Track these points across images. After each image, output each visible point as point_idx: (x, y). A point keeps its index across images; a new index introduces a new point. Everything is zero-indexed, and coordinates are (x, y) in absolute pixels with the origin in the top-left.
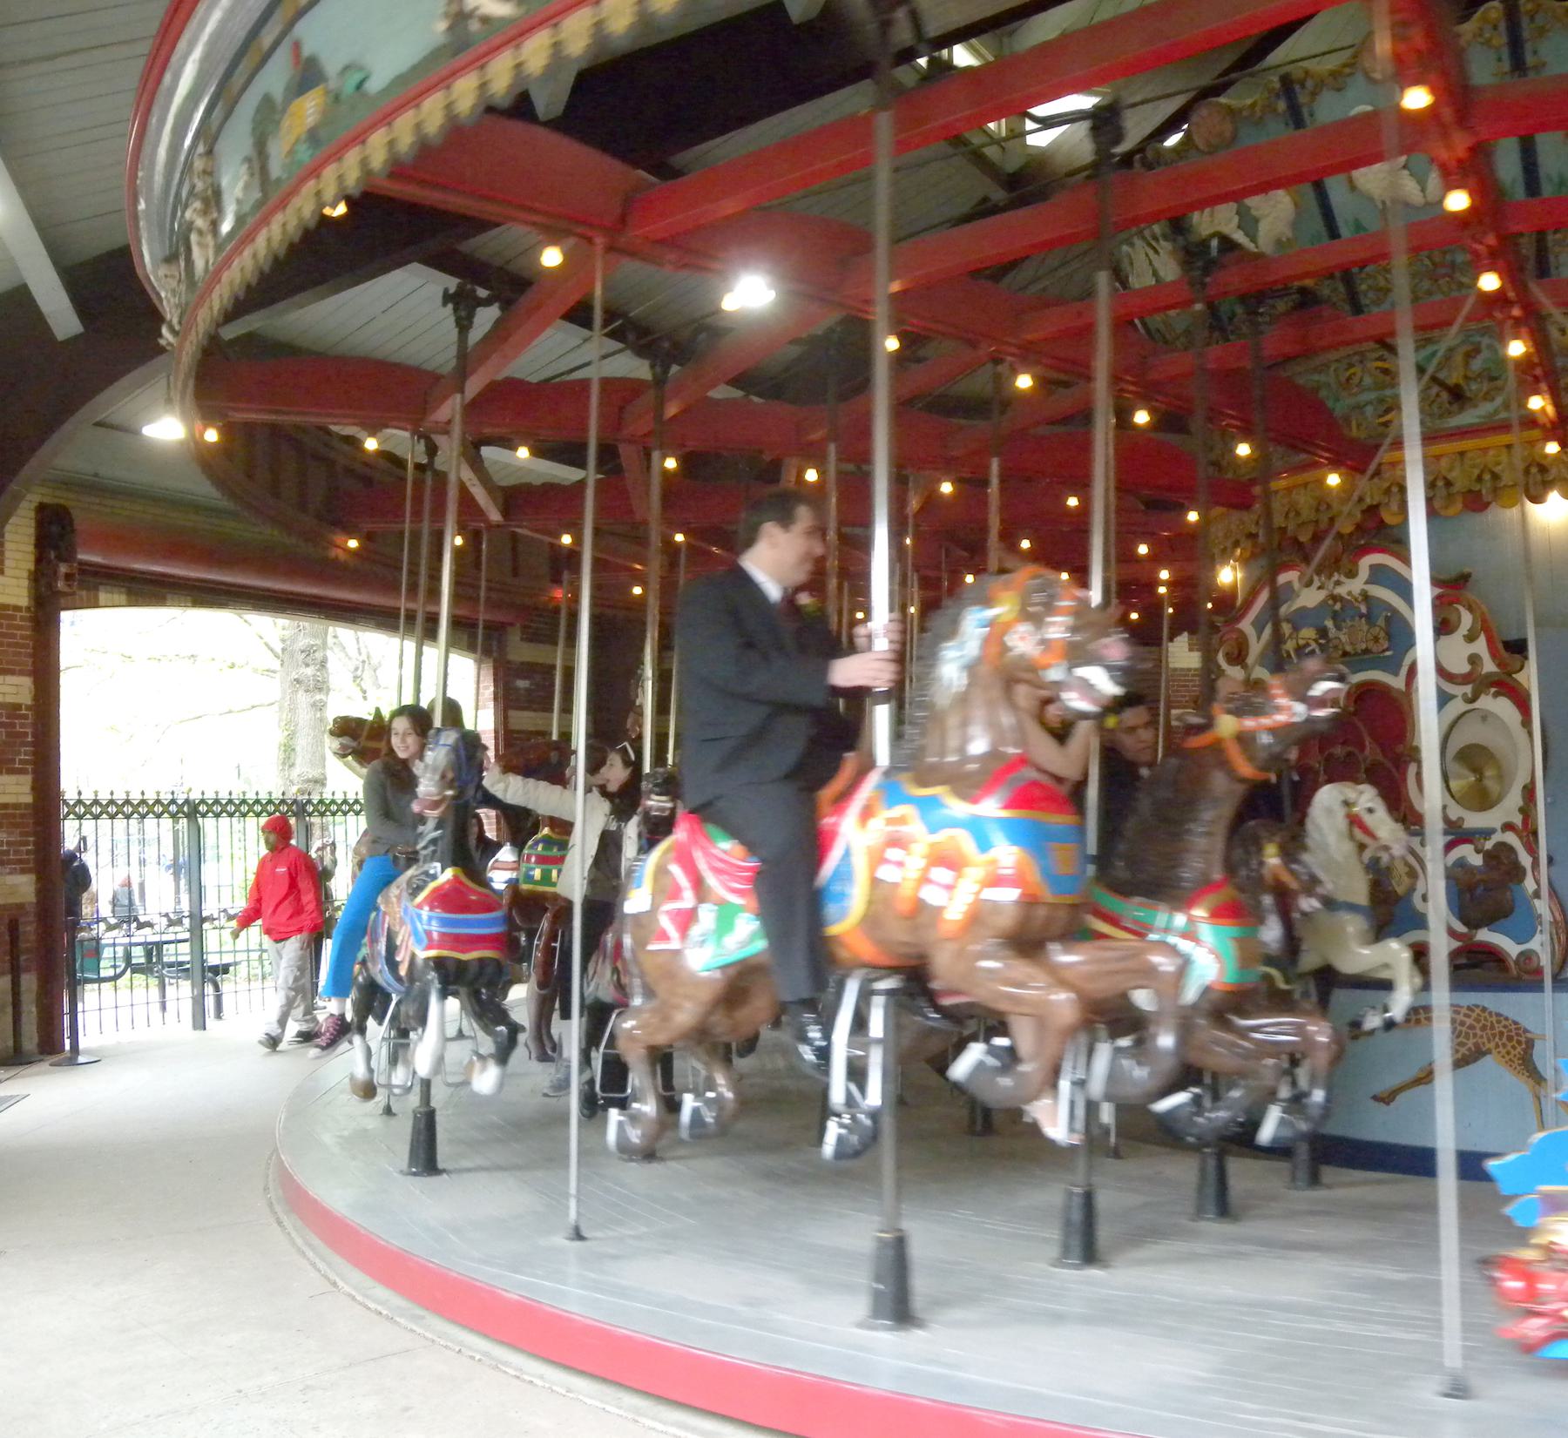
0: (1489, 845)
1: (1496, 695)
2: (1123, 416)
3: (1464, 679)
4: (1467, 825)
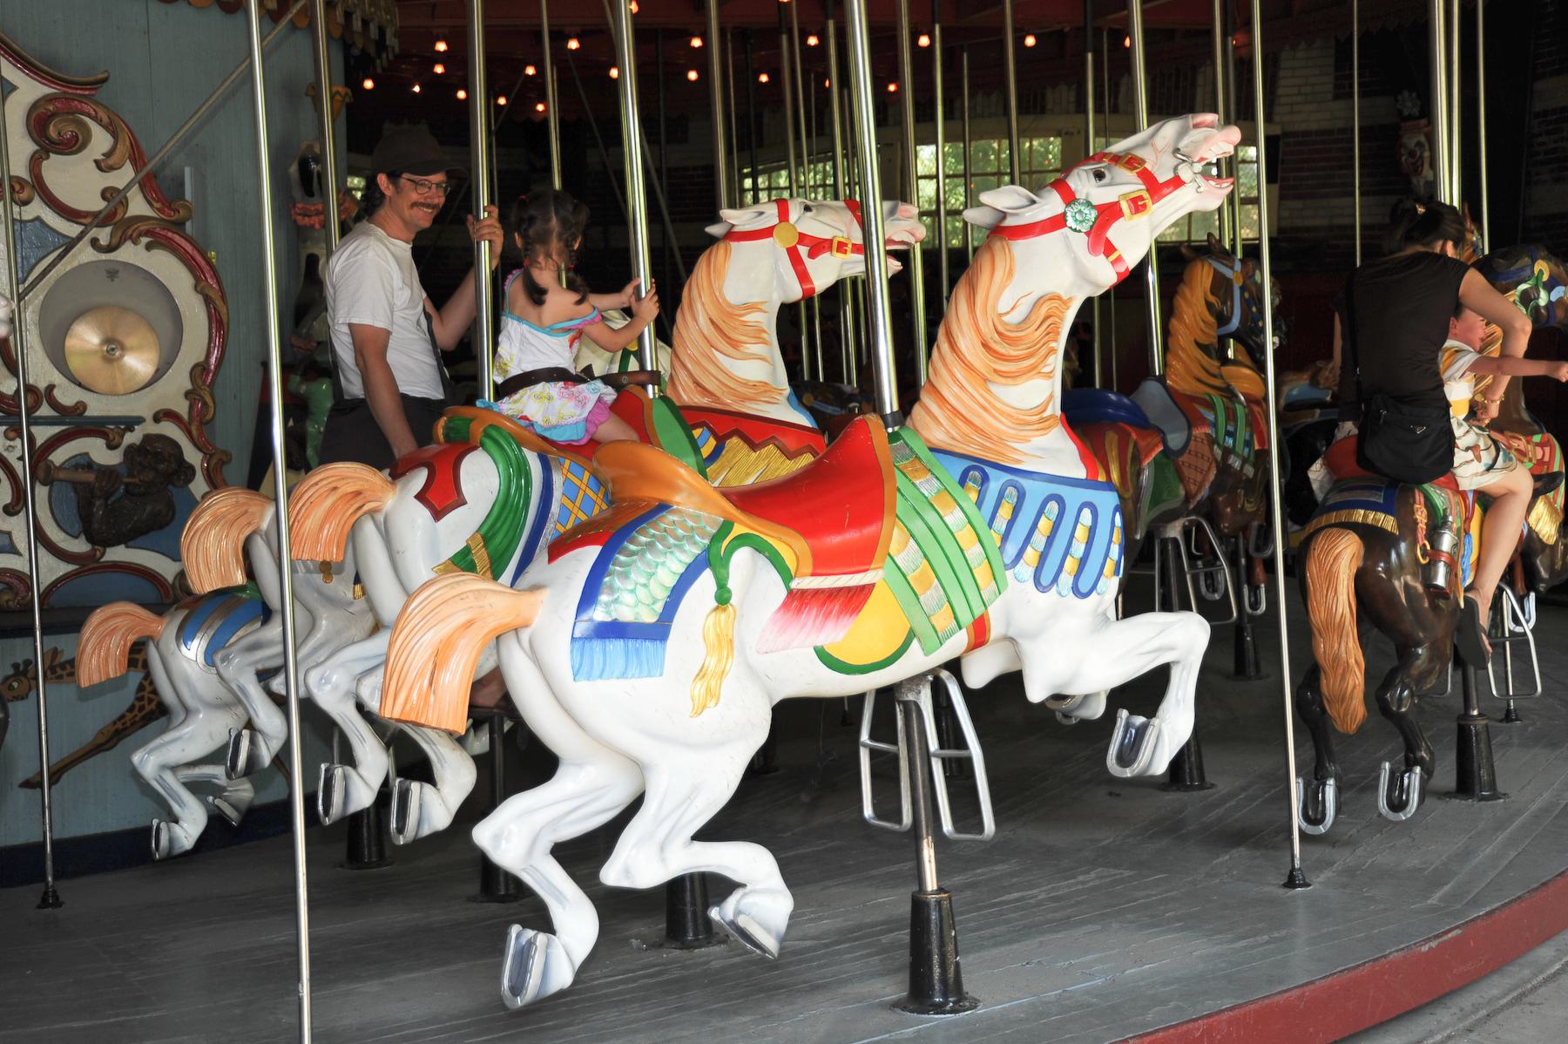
0: (133, 438)
1: (149, 247)
2: (1019, 41)
3: (101, 219)
4: (92, 411)
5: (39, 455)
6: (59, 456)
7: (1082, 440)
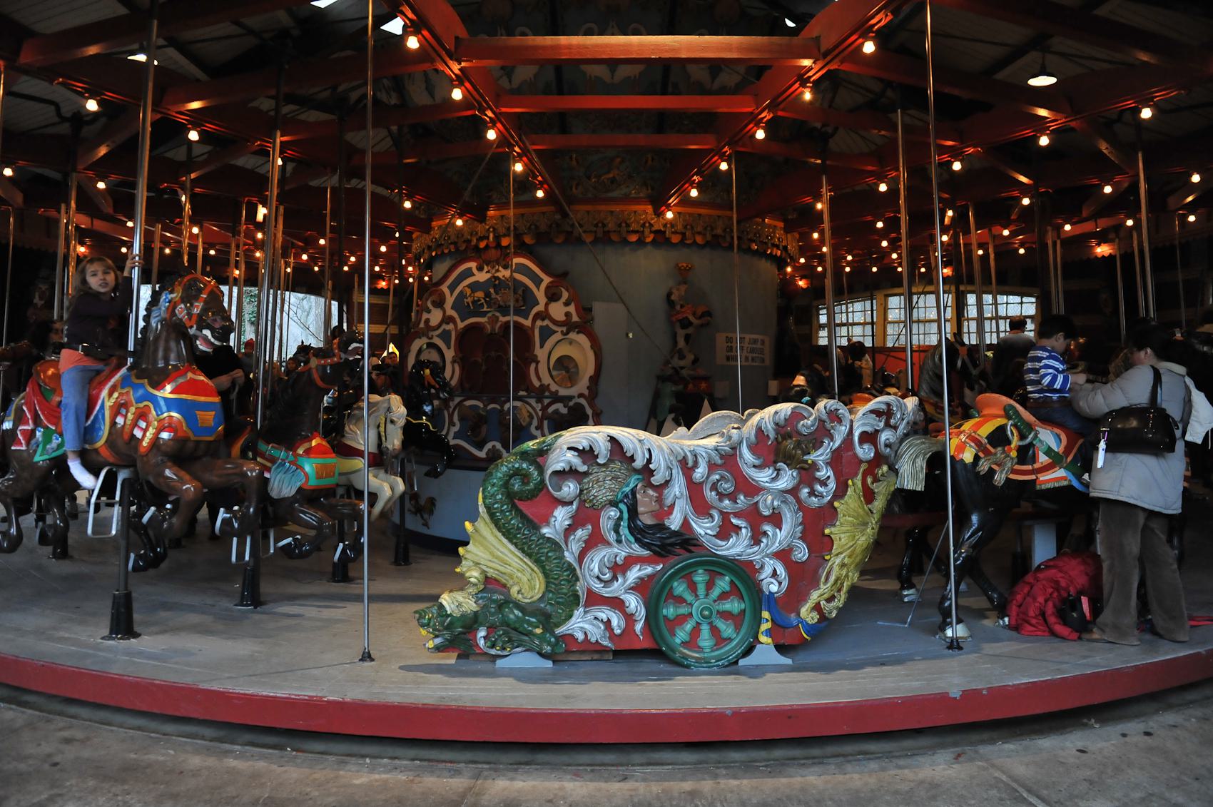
0: (571, 404)
1: (578, 333)
4: (560, 394)
5: (544, 409)
6: (551, 410)
7: (1136, 716)
